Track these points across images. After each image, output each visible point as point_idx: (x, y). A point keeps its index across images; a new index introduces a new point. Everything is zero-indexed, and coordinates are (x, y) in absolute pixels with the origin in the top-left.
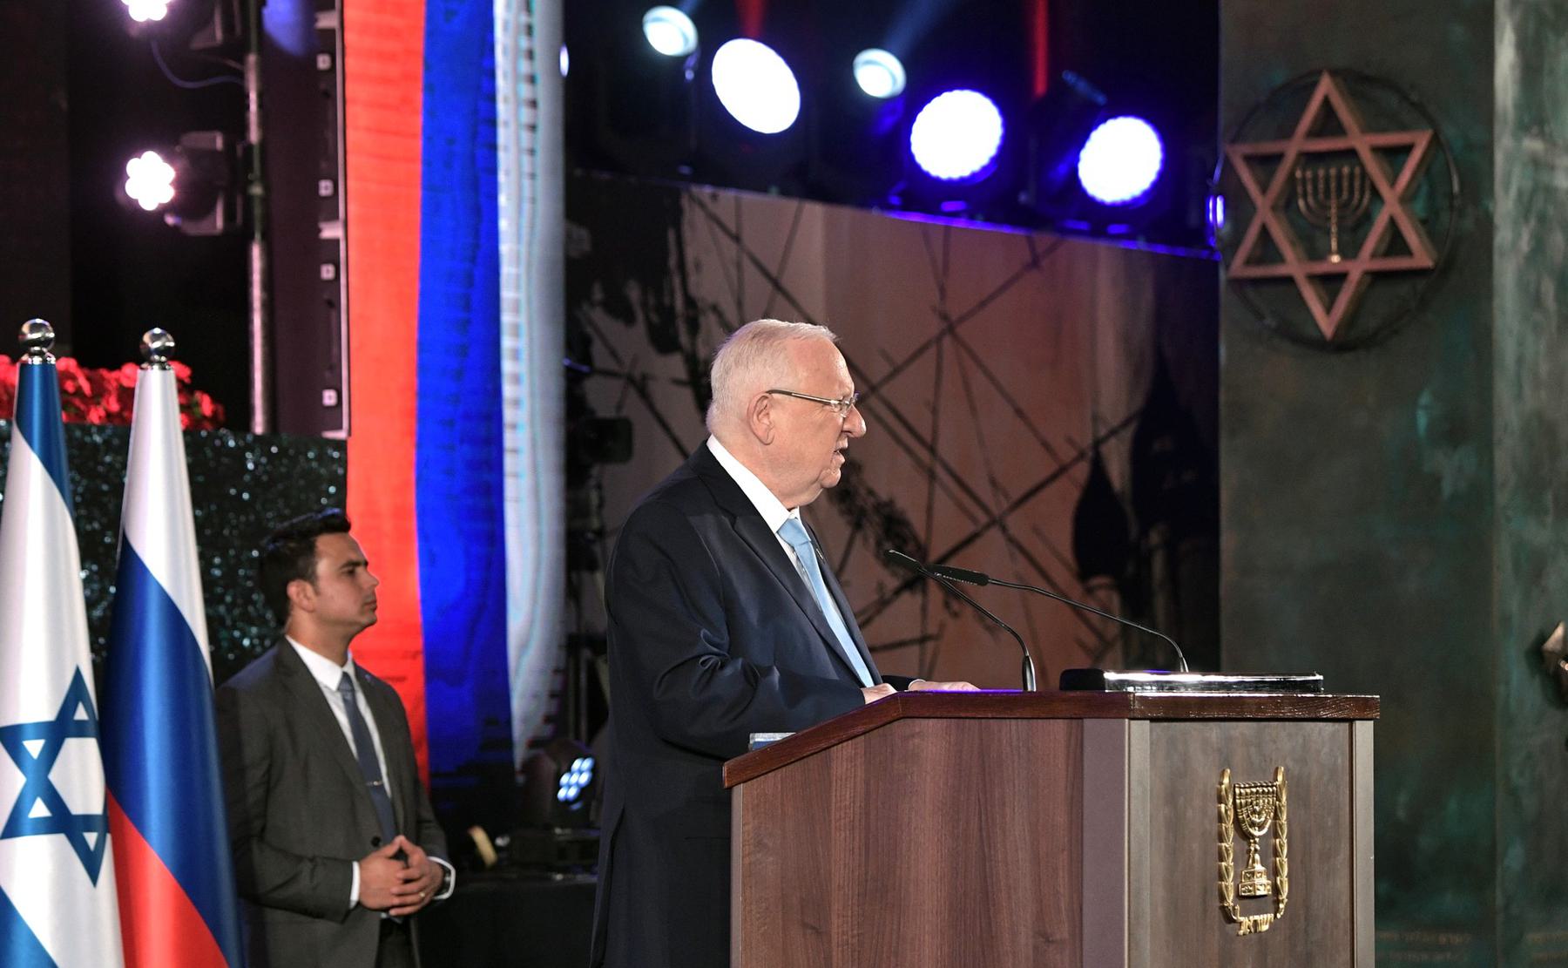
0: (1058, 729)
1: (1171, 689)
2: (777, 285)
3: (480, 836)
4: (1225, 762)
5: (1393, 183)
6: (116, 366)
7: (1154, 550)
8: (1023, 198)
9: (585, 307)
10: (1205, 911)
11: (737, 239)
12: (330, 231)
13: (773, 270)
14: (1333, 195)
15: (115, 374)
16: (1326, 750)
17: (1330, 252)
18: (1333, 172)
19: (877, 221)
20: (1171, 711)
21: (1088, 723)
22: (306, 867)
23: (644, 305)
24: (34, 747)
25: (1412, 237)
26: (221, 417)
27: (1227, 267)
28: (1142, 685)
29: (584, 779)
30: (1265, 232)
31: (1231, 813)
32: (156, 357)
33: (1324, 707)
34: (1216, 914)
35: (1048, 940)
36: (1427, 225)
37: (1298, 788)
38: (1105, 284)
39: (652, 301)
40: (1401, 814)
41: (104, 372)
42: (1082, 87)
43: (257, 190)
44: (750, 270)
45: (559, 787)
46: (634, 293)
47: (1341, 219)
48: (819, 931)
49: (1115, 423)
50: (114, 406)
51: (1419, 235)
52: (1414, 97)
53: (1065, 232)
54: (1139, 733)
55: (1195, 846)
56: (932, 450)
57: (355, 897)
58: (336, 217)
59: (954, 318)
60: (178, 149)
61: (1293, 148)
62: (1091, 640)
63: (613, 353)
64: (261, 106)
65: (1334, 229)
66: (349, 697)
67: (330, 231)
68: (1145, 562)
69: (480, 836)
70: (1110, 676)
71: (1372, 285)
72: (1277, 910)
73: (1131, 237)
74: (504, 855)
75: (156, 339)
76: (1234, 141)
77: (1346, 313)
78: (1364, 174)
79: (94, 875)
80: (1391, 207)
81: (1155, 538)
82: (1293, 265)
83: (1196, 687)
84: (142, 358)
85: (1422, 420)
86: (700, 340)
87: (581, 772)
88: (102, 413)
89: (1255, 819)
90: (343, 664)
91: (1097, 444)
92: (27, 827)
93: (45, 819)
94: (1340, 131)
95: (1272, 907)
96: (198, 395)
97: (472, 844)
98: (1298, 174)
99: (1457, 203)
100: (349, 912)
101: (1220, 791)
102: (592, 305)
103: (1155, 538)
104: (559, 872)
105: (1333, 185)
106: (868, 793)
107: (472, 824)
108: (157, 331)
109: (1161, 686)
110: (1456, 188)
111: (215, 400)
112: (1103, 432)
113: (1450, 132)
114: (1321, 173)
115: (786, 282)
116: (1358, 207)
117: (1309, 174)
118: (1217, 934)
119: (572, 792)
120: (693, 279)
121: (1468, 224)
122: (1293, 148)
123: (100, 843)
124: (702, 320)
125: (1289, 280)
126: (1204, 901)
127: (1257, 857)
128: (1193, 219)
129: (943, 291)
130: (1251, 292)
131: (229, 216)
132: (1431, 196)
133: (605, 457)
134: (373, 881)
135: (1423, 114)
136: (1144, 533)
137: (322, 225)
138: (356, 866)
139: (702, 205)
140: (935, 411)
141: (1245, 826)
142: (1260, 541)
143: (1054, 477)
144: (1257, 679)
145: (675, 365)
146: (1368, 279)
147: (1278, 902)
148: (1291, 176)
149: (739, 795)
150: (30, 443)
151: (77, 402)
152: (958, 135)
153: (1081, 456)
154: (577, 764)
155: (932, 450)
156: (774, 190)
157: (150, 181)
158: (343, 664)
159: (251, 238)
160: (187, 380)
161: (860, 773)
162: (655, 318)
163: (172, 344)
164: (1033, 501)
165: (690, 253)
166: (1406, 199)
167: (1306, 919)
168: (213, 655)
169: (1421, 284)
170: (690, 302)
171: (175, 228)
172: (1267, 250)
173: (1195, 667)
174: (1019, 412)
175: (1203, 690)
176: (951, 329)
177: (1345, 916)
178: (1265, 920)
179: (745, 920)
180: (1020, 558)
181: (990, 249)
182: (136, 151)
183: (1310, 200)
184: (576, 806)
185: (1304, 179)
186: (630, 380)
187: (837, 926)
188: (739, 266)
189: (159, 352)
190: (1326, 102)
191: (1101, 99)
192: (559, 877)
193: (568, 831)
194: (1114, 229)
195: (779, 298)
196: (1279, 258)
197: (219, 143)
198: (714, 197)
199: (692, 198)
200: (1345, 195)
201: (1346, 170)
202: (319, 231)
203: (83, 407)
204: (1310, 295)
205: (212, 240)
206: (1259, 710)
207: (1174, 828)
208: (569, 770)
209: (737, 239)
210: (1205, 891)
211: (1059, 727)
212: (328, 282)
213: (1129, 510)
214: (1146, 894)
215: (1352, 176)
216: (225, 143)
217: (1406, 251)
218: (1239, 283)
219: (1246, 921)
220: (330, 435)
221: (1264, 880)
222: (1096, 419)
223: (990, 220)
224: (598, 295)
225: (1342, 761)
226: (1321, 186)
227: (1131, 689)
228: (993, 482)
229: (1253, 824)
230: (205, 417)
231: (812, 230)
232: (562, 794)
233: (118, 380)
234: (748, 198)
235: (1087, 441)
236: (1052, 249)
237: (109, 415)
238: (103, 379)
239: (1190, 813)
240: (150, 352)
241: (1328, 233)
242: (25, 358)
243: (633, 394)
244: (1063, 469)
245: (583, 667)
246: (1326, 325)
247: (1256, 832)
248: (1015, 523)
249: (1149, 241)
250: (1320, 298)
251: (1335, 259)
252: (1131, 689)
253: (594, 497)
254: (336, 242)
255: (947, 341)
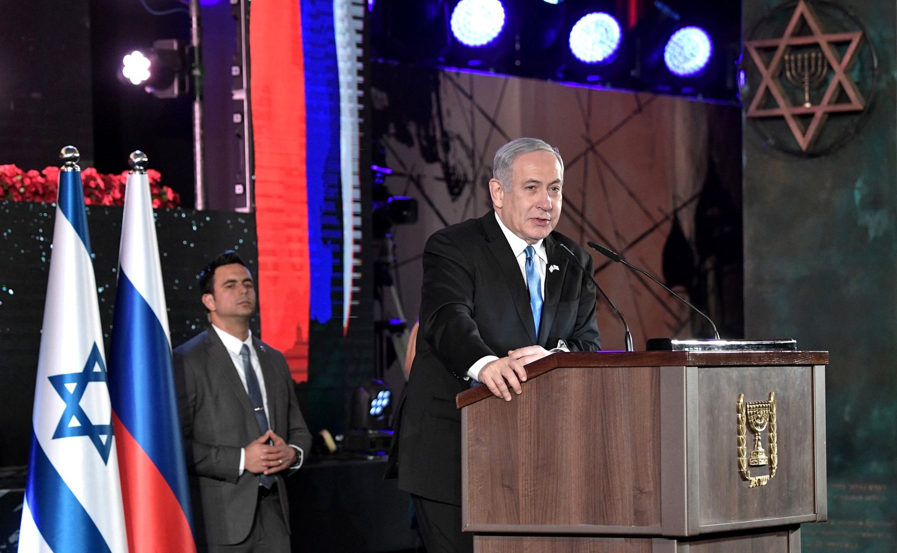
0: (645, 373)
1: (710, 349)
2: (493, 123)
3: (327, 436)
4: (741, 390)
5: (840, 62)
6: (119, 172)
7: (708, 273)
8: (633, 73)
9: (385, 136)
10: (730, 474)
11: (471, 98)
12: (239, 95)
13: (492, 116)
14: (806, 69)
15: (118, 177)
16: (798, 382)
17: (805, 102)
18: (806, 56)
19: (551, 88)
20: (709, 362)
21: (662, 368)
22: (213, 451)
23: (419, 135)
24: (71, 387)
25: (851, 92)
26: (178, 201)
27: (747, 111)
28: (693, 346)
29: (385, 402)
30: (767, 90)
31: (745, 419)
32: (137, 167)
33: (798, 358)
34: (737, 476)
35: (641, 492)
36: (859, 85)
37: (783, 403)
38: (680, 122)
39: (423, 133)
40: (847, 418)
41: (112, 176)
42: (666, 10)
43: (197, 72)
44: (478, 115)
45: (371, 407)
46: (412, 129)
47: (810, 82)
48: (512, 489)
49: (686, 198)
50: (118, 195)
51: (854, 90)
52: (852, 13)
53: (657, 92)
54: (692, 374)
55: (725, 437)
56: (582, 215)
57: (242, 467)
58: (242, 87)
59: (594, 140)
60: (152, 49)
61: (783, 43)
62: (672, 321)
63: (401, 163)
64: (199, 25)
65: (807, 88)
66: (246, 360)
67: (239, 95)
68: (703, 277)
69: (327, 436)
70: (675, 342)
71: (828, 120)
72: (771, 473)
73: (694, 95)
74: (340, 446)
75: (137, 157)
76: (750, 39)
77: (814, 136)
78: (824, 57)
79: (106, 460)
80: (838, 76)
81: (709, 264)
82: (784, 109)
83: (724, 348)
84: (131, 167)
85: (858, 196)
86: (450, 156)
87: (383, 399)
88: (111, 199)
89: (758, 422)
90: (244, 340)
91: (676, 211)
92: (67, 432)
93: (78, 427)
94: (810, 33)
95: (768, 471)
96: (165, 189)
97: (322, 440)
98: (786, 57)
99: (876, 73)
100: (239, 477)
101: (738, 406)
102: (389, 136)
103: (709, 264)
104: (371, 455)
105: (806, 63)
106: (538, 409)
107: (322, 429)
108: (138, 152)
109: (704, 347)
110: (876, 64)
111: (175, 191)
112: (679, 204)
113: (872, 33)
114: (799, 56)
115: (499, 122)
116: (819, 77)
117: (792, 57)
118: (737, 488)
119: (379, 410)
120: (446, 121)
121: (883, 85)
122: (783, 43)
123: (109, 441)
124: (452, 144)
125: (781, 118)
126: (730, 469)
127: (760, 443)
128: (729, 84)
129: (587, 126)
130: (760, 125)
131: (182, 87)
132: (862, 70)
133: (402, 220)
134: (252, 458)
135: (857, 23)
136: (702, 261)
137: (234, 92)
138: (243, 451)
139: (451, 79)
140: (584, 194)
141: (753, 426)
142: (767, 264)
143: (651, 230)
144: (772, 342)
145: (436, 170)
146: (827, 116)
147: (772, 468)
148: (783, 58)
149: (465, 412)
150: (66, 216)
151: (97, 193)
152: (594, 38)
153: (667, 218)
154: (381, 394)
155: (582, 215)
156: (492, 70)
157: (136, 68)
158: (244, 340)
159: (194, 99)
160: (159, 180)
161: (534, 399)
162: (425, 143)
163: (146, 160)
164: (639, 245)
165: (444, 106)
166: (848, 71)
167: (788, 477)
168: (172, 336)
169: (856, 119)
170: (445, 134)
171: (151, 94)
172: (769, 100)
173: (723, 337)
174: (631, 194)
175: (727, 349)
176: (592, 148)
177: (810, 475)
178: (765, 479)
179: (469, 483)
180: (633, 276)
181: (614, 101)
182: (128, 50)
183: (793, 72)
184: (381, 418)
185: (790, 61)
186: (411, 178)
187: (523, 486)
188: (472, 113)
189: (140, 164)
190: (802, 16)
191: (677, 17)
192: (371, 458)
193: (376, 432)
194: (685, 90)
195: (495, 131)
196: (776, 106)
197: (175, 46)
198: (458, 74)
199: (445, 75)
200: (813, 69)
201: (813, 55)
202: (232, 95)
203: (100, 196)
204: (794, 126)
205: (171, 101)
206: (760, 360)
207: (712, 427)
208: (376, 398)
209: (471, 98)
210: (730, 465)
211: (646, 372)
212: (238, 124)
213: (694, 248)
214: (697, 466)
215: (817, 59)
216: (179, 46)
217: (847, 100)
218: (754, 120)
219: (754, 480)
220: (240, 210)
221: (764, 456)
222: (675, 197)
223: (615, 86)
224: (392, 129)
225: (808, 388)
226: (799, 64)
227: (687, 349)
228: (617, 234)
229: (757, 425)
230: (169, 201)
231: (513, 92)
232: (372, 411)
233: (119, 180)
234: (478, 75)
235: (670, 210)
236: (649, 102)
237: (115, 200)
238: (111, 180)
239: (721, 419)
240: (134, 164)
241: (803, 90)
242: (63, 168)
243: (412, 185)
244: (656, 226)
245: (385, 339)
246: (802, 142)
247: (758, 429)
248: (630, 257)
249: (704, 96)
250: (800, 128)
251: (808, 105)
252: (687, 349)
253: (390, 244)
254: (242, 101)
255: (590, 154)
